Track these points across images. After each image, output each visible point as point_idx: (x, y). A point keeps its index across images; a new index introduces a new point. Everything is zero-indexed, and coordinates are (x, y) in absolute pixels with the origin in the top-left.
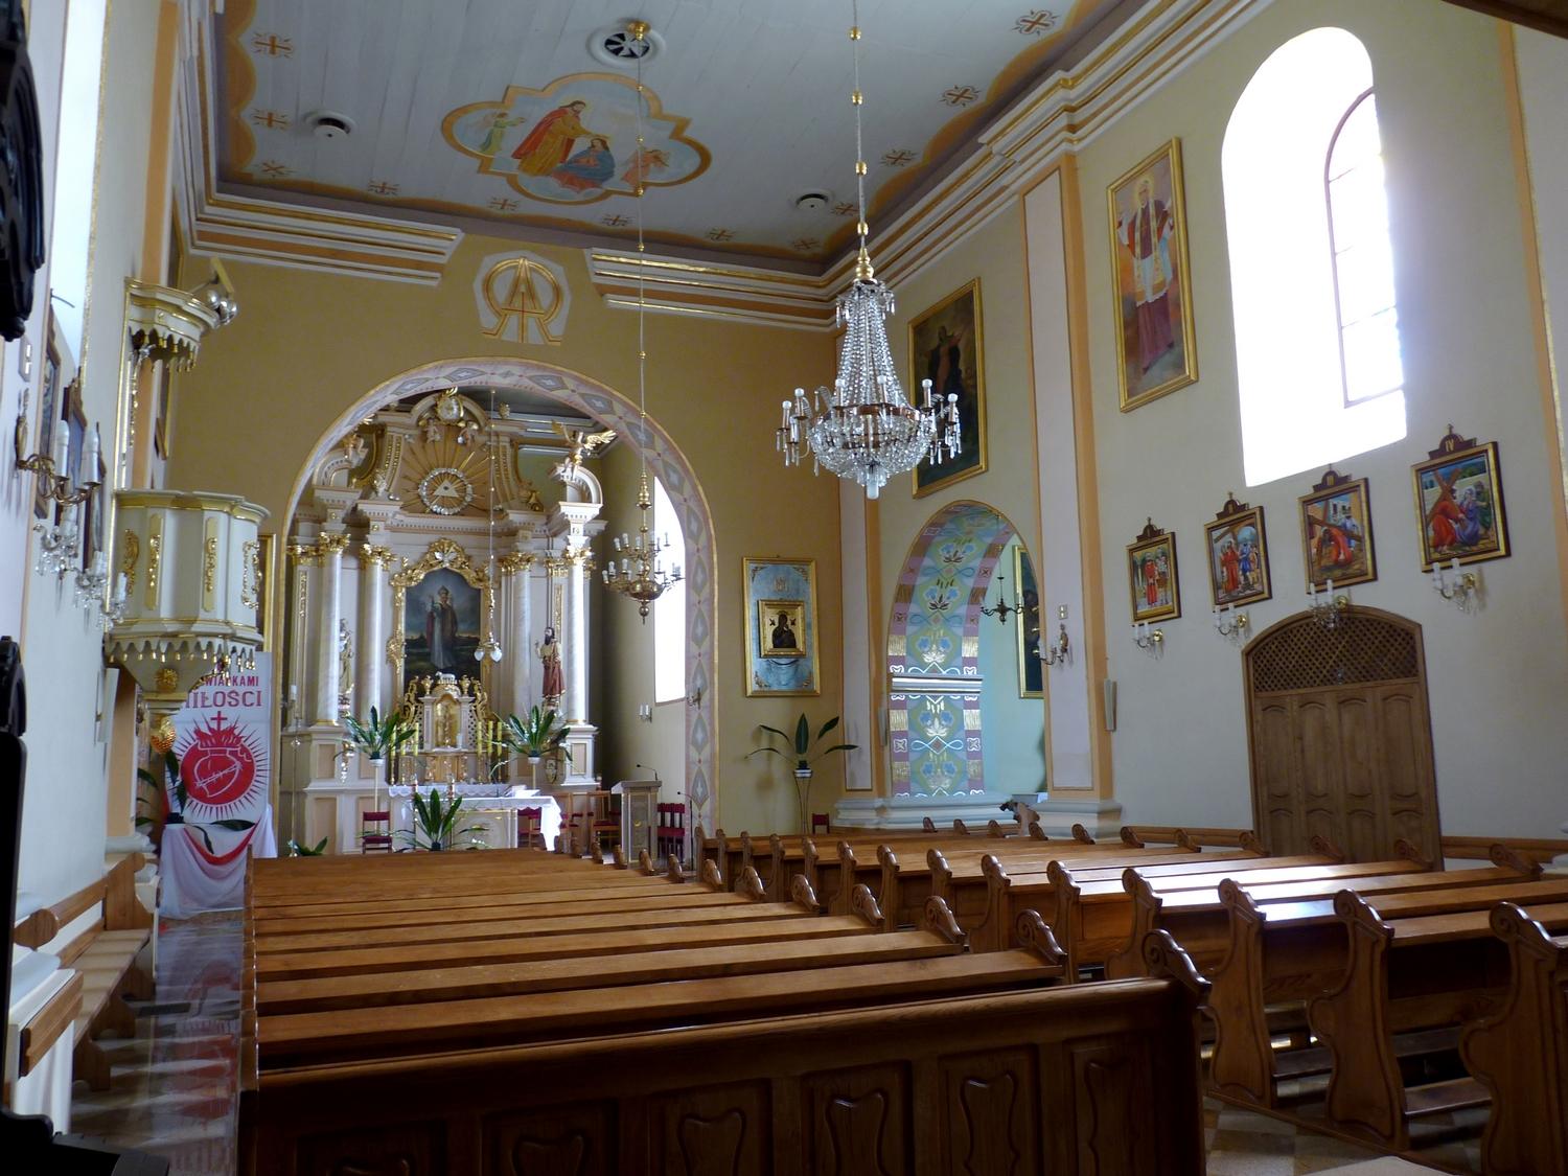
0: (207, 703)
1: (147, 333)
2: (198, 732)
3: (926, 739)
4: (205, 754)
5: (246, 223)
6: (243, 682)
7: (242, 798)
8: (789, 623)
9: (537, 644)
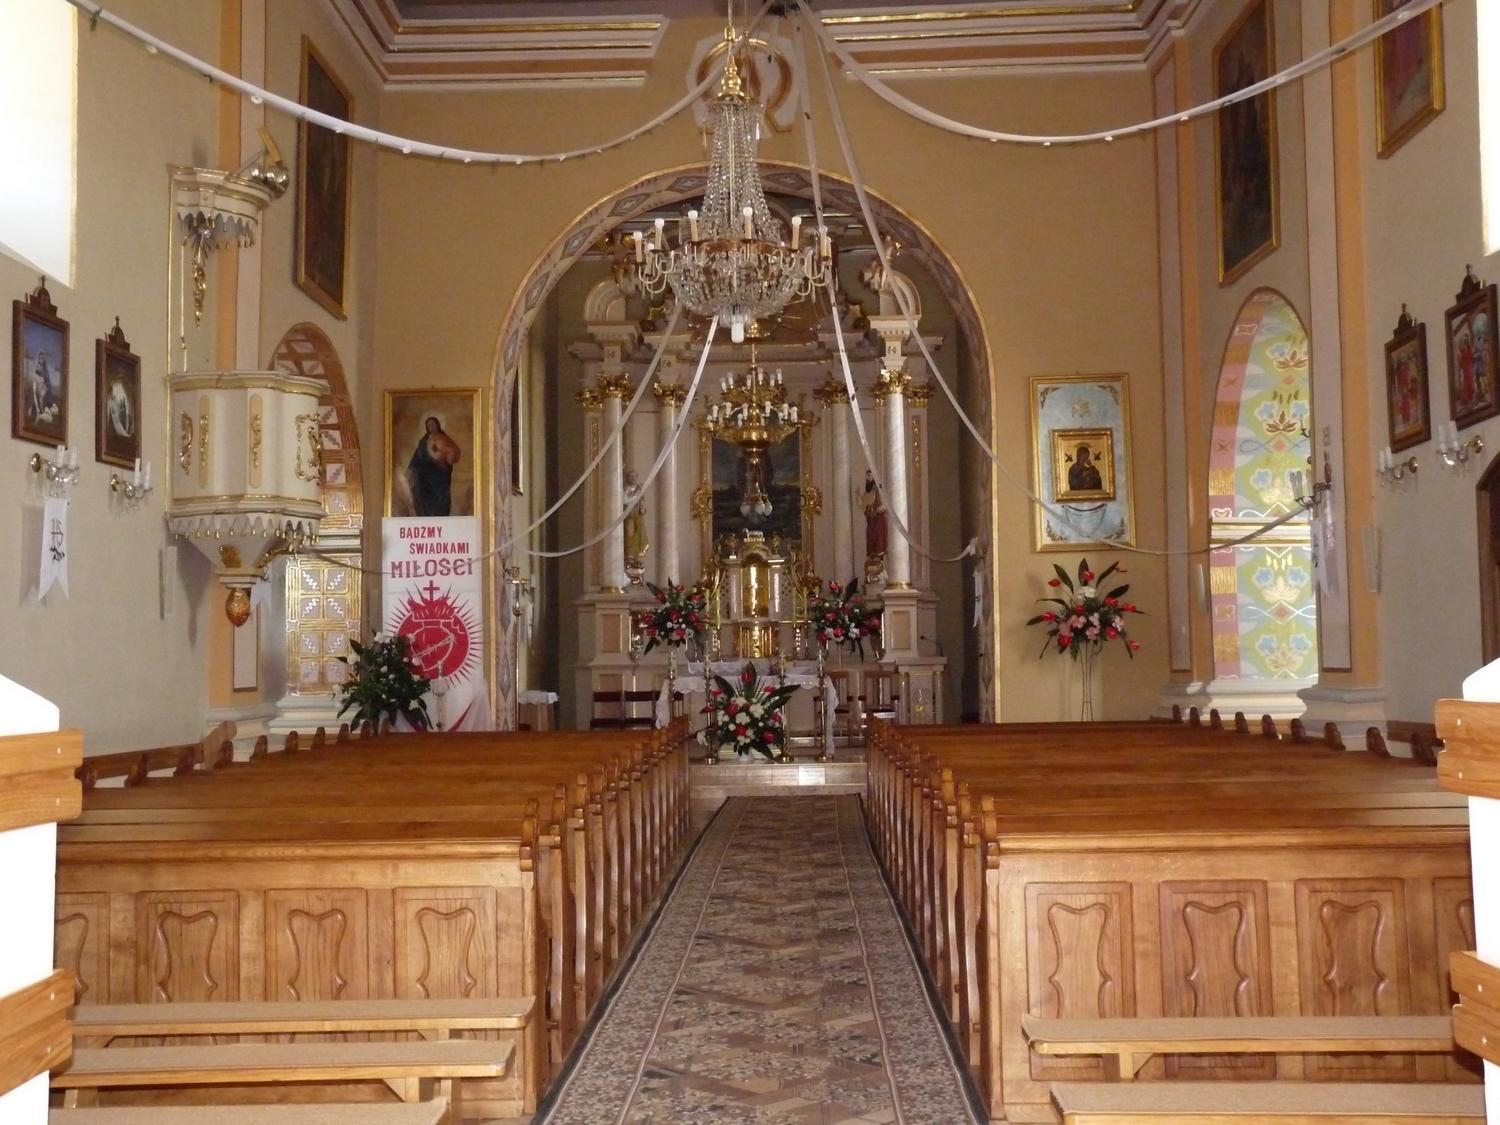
0: (420, 572)
1: (195, 216)
2: (411, 603)
3: (1266, 605)
4: (419, 625)
5: (411, 47)
6: (453, 550)
7: (457, 672)
8: (1091, 457)
9: (858, 492)
